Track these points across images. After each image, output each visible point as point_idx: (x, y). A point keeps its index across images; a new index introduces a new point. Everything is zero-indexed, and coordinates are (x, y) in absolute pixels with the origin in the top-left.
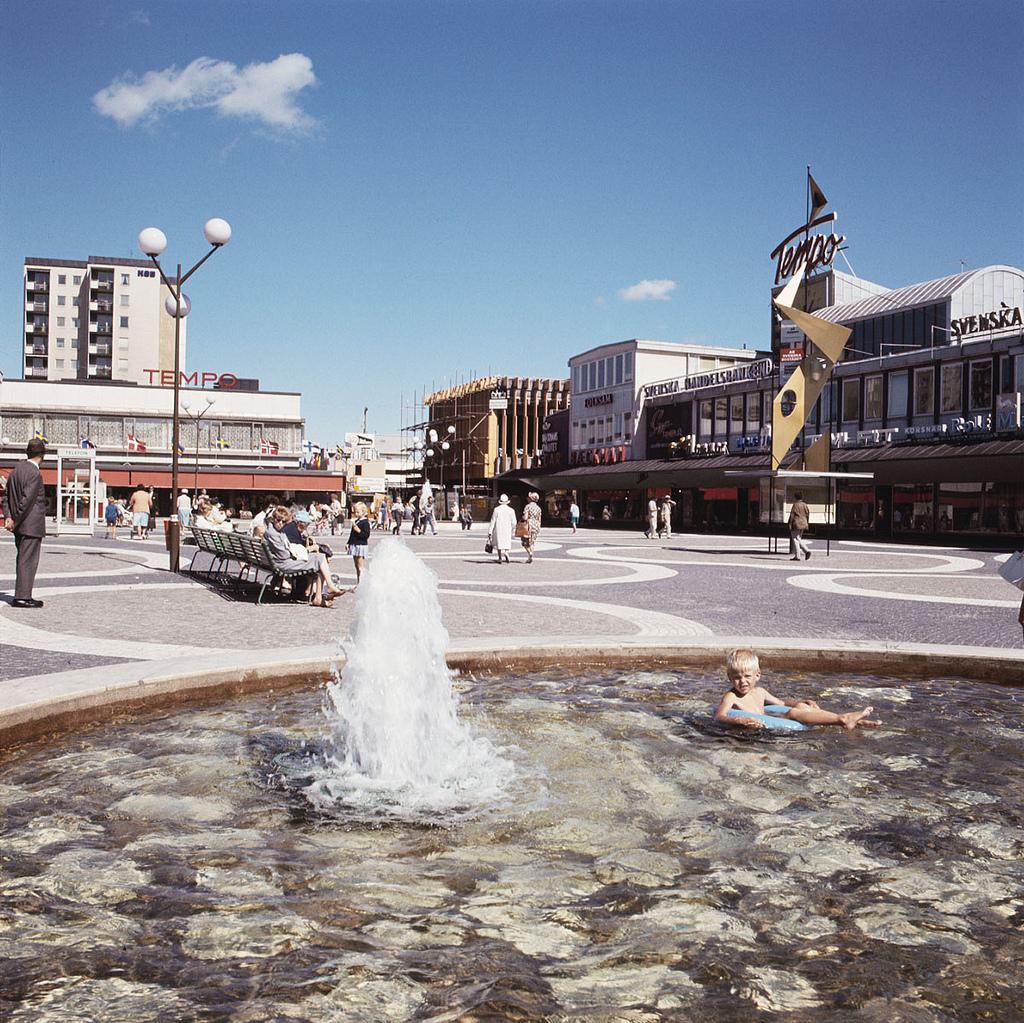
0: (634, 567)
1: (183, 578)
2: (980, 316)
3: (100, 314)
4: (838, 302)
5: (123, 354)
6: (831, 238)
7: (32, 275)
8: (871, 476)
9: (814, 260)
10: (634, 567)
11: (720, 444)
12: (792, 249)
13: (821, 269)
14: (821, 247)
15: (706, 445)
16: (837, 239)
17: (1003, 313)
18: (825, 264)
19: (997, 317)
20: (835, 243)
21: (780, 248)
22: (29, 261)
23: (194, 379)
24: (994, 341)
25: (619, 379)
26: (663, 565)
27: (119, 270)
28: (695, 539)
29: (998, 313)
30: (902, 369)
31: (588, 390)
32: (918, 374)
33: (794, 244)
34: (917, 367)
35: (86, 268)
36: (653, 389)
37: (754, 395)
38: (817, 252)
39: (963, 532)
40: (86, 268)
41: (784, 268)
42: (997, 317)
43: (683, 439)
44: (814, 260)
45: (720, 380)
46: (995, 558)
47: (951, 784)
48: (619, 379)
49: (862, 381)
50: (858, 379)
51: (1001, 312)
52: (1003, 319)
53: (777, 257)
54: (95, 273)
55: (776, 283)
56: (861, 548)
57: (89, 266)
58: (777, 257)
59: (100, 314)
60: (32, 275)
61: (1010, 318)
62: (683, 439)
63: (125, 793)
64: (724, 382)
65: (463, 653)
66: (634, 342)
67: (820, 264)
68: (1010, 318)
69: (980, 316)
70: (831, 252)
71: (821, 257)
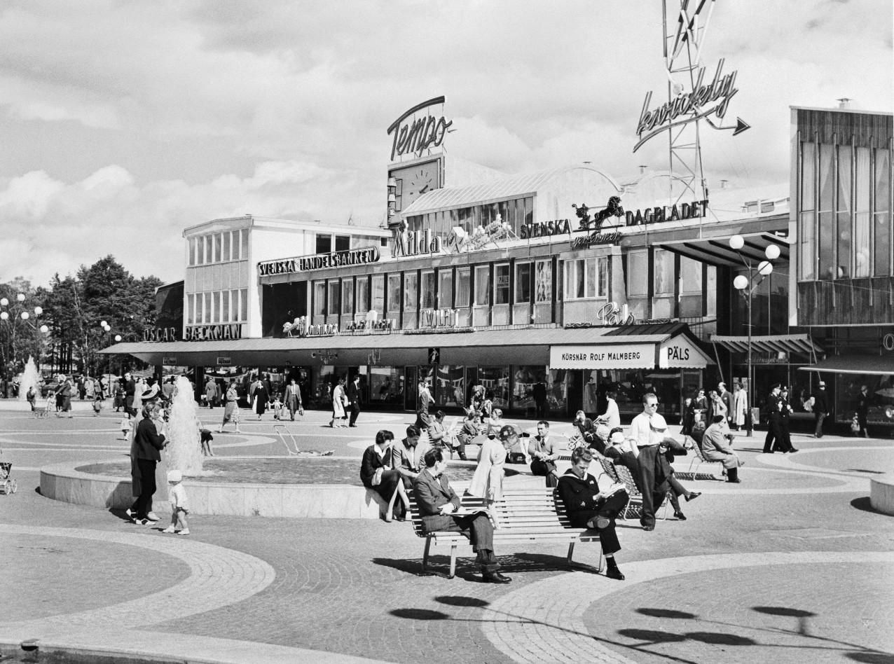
0: (247, 437)
1: (672, 246)
2: (542, 223)
6: (442, 120)
9: (427, 140)
10: (247, 437)
14: (434, 126)
15: (319, 327)
17: (558, 223)
18: (437, 145)
19: (554, 226)
20: (445, 126)
21: (395, 126)
23: (672, 141)
25: (236, 255)
26: (267, 436)
29: (554, 222)
30: (484, 264)
31: (231, 259)
32: (518, 265)
33: (409, 122)
36: (269, 267)
37: (379, 277)
38: (430, 132)
39: (834, 292)
41: (400, 145)
42: (554, 226)
44: (427, 140)
45: (333, 262)
48: (236, 255)
50: (508, 264)
51: (556, 221)
52: (557, 227)
53: (393, 133)
61: (562, 227)
67: (432, 144)
68: (562, 227)
69: (542, 223)
71: (433, 138)
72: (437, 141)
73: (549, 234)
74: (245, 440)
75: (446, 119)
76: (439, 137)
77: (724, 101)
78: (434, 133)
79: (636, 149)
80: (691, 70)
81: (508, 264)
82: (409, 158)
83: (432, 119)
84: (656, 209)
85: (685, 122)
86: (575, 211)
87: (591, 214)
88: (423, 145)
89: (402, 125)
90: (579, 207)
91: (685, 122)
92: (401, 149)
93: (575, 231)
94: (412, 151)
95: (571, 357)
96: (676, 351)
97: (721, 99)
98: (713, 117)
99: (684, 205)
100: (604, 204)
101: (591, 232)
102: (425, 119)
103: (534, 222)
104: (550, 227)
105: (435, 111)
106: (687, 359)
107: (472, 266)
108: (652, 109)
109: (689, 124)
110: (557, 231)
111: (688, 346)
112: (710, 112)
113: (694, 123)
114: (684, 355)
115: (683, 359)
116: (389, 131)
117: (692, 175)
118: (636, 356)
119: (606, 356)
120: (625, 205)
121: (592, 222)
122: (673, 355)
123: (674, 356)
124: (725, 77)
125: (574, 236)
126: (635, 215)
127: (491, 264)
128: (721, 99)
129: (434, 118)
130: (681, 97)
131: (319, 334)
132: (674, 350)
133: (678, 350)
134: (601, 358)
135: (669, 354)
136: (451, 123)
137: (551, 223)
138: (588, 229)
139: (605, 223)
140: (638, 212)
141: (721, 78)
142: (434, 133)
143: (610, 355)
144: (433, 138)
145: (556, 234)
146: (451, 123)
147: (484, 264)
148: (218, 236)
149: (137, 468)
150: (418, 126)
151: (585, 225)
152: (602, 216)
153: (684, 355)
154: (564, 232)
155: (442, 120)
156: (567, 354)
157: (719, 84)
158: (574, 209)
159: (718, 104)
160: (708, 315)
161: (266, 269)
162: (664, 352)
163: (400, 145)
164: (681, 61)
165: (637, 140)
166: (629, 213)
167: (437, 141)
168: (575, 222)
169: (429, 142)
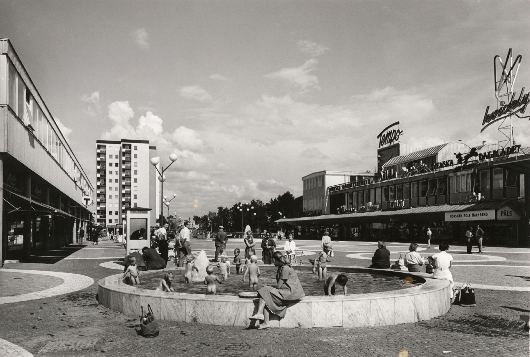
3: (126, 178)
4: (400, 155)
5: (136, 189)
6: (399, 130)
7: (99, 147)
8: (522, 177)
9: (393, 138)
11: (354, 209)
12: (385, 135)
13: (395, 142)
14: (395, 133)
16: (400, 131)
18: (396, 140)
19: (446, 163)
20: (400, 133)
21: (380, 135)
22: (98, 142)
24: (445, 171)
27: (133, 145)
28: (345, 243)
30: (416, 181)
33: (386, 133)
34: (421, 180)
35: (120, 144)
40: (120, 144)
41: (382, 141)
42: (446, 163)
43: (341, 207)
44: (393, 138)
46: (435, 248)
47: (84, 326)
49: (403, 185)
50: (425, 181)
52: (447, 163)
53: (380, 138)
54: (124, 146)
55: (379, 147)
56: (397, 245)
57: (122, 143)
58: (380, 138)
59: (126, 178)
60: (99, 147)
62: (341, 207)
63: (70, 299)
64: (356, 186)
65: (230, 295)
66: (325, 172)
67: (395, 140)
70: (399, 136)
71: (395, 137)
72: (397, 139)
73: (443, 167)
74: (299, 248)
75: (400, 130)
76: (397, 137)
77: (524, 106)
78: (395, 135)
79: (482, 130)
80: (508, 95)
81: (425, 181)
82: (386, 146)
83: (394, 131)
84: (494, 151)
85: (505, 117)
86: (455, 156)
87: (463, 156)
88: (391, 141)
89: (383, 135)
90: (457, 154)
91: (505, 117)
92: (382, 143)
93: (455, 164)
94: (387, 143)
95: (454, 216)
96: (505, 213)
97: (523, 105)
98: (519, 114)
99: (508, 148)
100: (468, 151)
101: (463, 164)
102: (392, 131)
103: (437, 162)
104: (445, 164)
105: (396, 128)
106: (511, 216)
107: (410, 183)
108: (490, 113)
109: (507, 118)
110: (447, 165)
111: (510, 210)
112: (517, 111)
113: (510, 117)
114: (509, 214)
115: (509, 216)
116: (378, 137)
117: (508, 139)
118: (486, 214)
119: (471, 215)
120: (478, 152)
121: (463, 160)
122: (504, 214)
123: (504, 215)
124: (525, 95)
125: (455, 167)
126: (483, 154)
127: (418, 181)
128: (523, 105)
129: (395, 130)
130: (503, 106)
131: (348, 212)
132: (504, 212)
133: (506, 212)
134: (469, 216)
135: (502, 214)
136: (402, 131)
137: (444, 162)
138: (462, 163)
139: (469, 160)
140: (485, 153)
141: (523, 96)
142: (395, 135)
143: (473, 215)
144: (395, 137)
145: (447, 166)
146: (402, 131)
147: (416, 181)
148: (313, 178)
149: (15, 248)
150: (389, 134)
151: (460, 162)
152: (467, 157)
153: (509, 214)
154: (450, 165)
155: (399, 130)
156: (453, 215)
157: (522, 99)
158: (455, 155)
159: (522, 107)
160: (521, 196)
161: (330, 189)
162: (499, 213)
163: (382, 141)
164: (503, 91)
165: (483, 127)
166: (481, 154)
167: (397, 139)
168: (456, 161)
169: (393, 139)
